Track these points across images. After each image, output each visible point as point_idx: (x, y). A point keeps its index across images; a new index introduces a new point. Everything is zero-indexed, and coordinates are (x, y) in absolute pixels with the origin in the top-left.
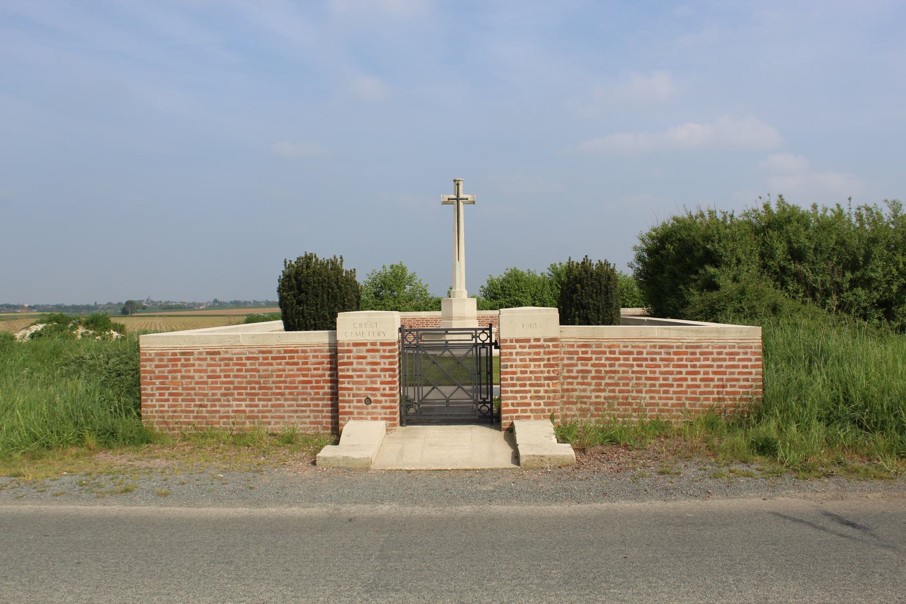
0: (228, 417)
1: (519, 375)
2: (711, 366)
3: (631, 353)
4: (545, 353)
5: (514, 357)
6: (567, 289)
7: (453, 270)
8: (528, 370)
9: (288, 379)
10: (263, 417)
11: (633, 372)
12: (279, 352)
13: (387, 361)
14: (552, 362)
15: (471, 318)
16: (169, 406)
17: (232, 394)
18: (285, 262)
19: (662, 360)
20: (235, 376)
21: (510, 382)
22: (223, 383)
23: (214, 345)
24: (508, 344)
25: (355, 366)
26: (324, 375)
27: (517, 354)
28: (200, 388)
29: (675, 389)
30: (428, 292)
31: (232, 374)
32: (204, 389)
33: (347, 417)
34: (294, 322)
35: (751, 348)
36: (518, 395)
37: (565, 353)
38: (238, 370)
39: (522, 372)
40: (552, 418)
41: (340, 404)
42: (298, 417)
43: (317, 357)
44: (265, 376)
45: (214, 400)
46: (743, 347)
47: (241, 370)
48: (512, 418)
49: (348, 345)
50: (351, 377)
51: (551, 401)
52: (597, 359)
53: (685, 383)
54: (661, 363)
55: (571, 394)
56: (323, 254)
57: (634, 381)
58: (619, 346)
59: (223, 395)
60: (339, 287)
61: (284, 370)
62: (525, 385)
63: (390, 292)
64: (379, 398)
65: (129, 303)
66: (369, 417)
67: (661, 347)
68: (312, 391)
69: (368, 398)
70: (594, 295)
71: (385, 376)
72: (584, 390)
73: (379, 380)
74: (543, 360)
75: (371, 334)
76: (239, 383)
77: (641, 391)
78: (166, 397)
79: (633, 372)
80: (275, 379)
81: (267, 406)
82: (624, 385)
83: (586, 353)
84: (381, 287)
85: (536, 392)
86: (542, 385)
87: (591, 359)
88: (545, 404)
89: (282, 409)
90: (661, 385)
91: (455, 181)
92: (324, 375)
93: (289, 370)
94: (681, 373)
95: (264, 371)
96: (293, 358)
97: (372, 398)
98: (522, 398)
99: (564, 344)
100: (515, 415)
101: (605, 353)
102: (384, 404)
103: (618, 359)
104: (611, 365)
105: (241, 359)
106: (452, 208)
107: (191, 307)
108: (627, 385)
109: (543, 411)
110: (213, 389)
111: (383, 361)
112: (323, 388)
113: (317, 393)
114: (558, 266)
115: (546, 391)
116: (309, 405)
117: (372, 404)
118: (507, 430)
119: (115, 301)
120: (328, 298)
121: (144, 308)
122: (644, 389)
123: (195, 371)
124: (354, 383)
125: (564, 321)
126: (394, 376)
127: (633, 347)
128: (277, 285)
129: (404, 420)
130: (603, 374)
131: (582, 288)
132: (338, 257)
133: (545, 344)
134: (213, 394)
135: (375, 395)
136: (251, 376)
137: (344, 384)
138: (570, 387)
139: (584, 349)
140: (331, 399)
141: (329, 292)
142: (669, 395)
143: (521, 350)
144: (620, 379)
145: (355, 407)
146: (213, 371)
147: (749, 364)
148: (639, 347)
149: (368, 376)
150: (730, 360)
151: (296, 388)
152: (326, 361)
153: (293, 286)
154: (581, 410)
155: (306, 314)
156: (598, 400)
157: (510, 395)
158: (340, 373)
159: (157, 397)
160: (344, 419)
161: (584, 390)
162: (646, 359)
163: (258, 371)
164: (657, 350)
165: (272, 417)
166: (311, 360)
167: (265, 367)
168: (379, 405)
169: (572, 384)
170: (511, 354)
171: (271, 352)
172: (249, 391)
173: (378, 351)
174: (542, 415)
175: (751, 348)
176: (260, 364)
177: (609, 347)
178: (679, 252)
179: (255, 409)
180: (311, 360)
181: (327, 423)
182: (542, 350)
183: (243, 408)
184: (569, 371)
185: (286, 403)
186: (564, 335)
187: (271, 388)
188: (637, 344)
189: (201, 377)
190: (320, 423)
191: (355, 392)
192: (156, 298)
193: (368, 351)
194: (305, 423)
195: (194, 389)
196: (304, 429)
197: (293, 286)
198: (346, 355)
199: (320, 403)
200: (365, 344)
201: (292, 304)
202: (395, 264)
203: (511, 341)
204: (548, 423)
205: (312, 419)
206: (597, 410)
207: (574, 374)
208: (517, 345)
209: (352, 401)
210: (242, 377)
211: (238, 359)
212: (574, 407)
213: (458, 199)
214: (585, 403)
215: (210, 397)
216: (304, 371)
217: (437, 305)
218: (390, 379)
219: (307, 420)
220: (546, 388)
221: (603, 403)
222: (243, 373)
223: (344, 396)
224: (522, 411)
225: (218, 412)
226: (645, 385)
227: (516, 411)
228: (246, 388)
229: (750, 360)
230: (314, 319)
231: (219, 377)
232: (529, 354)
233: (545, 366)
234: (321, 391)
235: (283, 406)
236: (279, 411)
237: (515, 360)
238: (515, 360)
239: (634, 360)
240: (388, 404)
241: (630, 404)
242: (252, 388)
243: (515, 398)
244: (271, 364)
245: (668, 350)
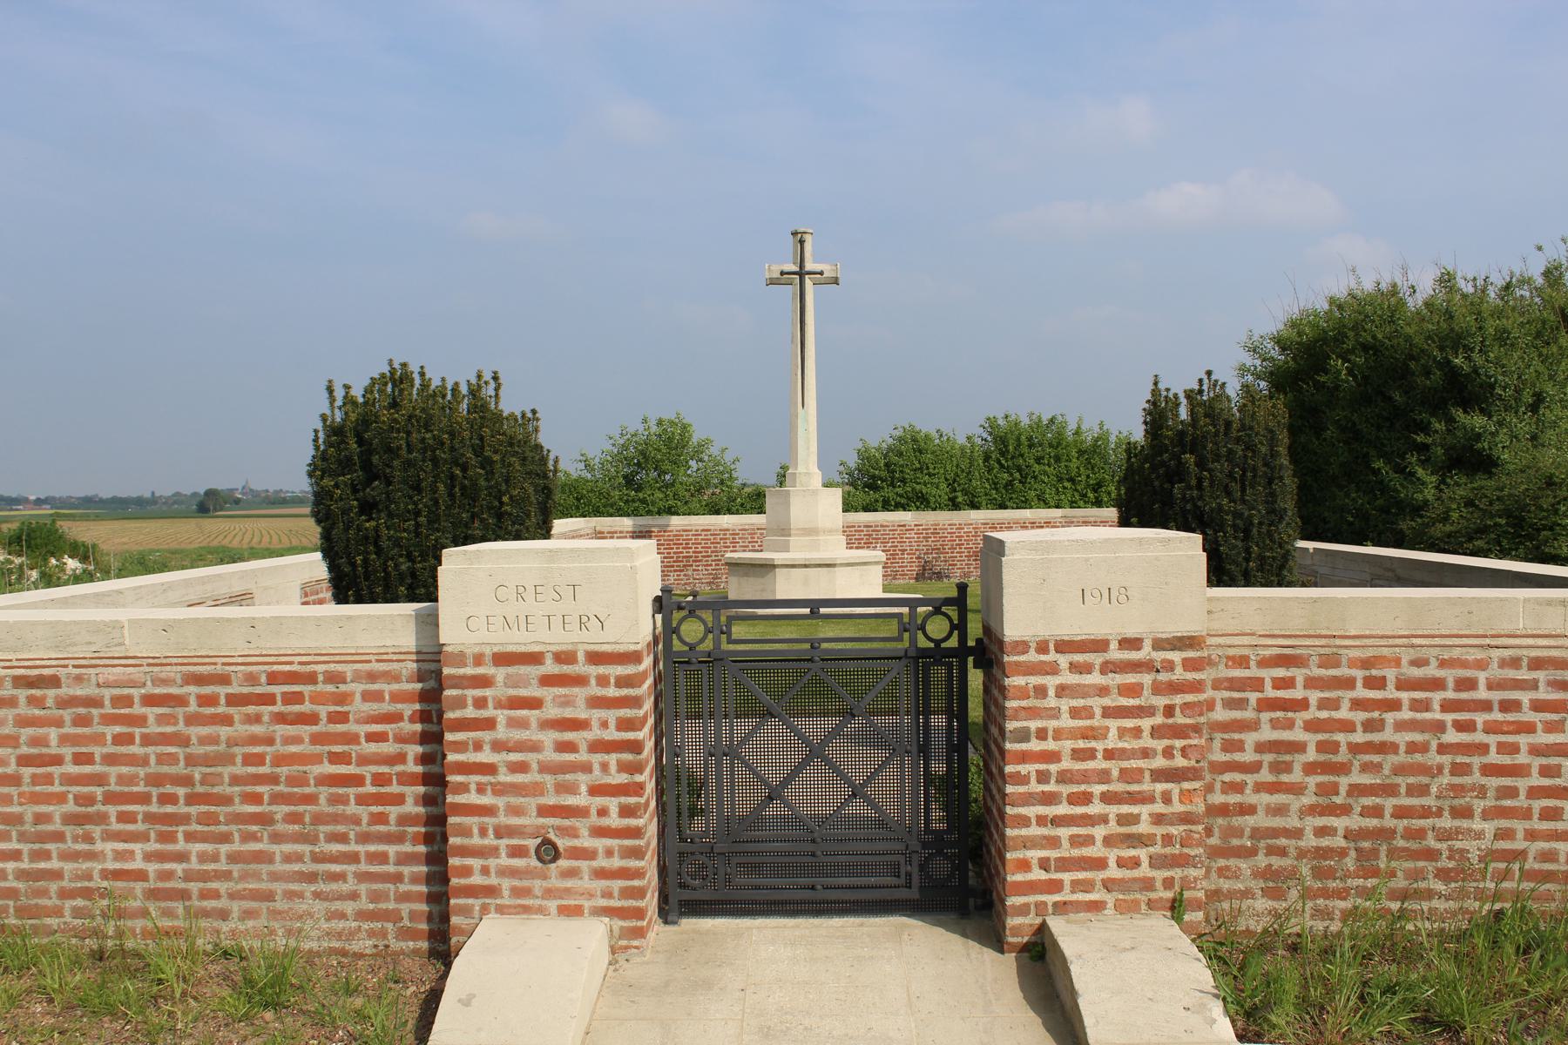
0: (87, 893)
1: (1066, 764)
3: (1437, 684)
4: (1157, 689)
5: (1051, 701)
6: (1154, 468)
7: (793, 428)
8: (1099, 746)
9: (284, 771)
10: (204, 895)
11: (1442, 749)
12: (252, 679)
13: (612, 715)
14: (1180, 719)
15: (831, 531)
17: (102, 818)
18: (330, 390)
19: (1538, 706)
20: (110, 759)
21: (1035, 787)
23: (40, 653)
24: (1032, 656)
25: (501, 732)
26: (400, 758)
27: (1062, 691)
30: (735, 475)
31: (98, 751)
33: (476, 903)
34: (353, 565)
36: (1064, 833)
37: (1217, 685)
38: (119, 740)
39: (1078, 755)
40: (1175, 908)
41: (454, 861)
42: (317, 895)
43: (376, 697)
44: (208, 761)
45: (42, 838)
47: (127, 739)
48: (1041, 908)
49: (478, 660)
50: (490, 769)
51: (1176, 850)
52: (1323, 704)
54: (1536, 717)
55: (1238, 821)
56: (447, 365)
57: (1446, 779)
58: (1397, 662)
59: (70, 819)
60: (487, 463)
61: (270, 741)
62: (1086, 799)
63: (653, 479)
64: (586, 842)
65: (210, 493)
66: (553, 905)
67: (1536, 664)
68: (364, 812)
69: (547, 842)
70: (1235, 487)
71: (605, 767)
72: (1280, 810)
74: (1148, 711)
75: (557, 622)
76: (121, 779)
77: (1466, 813)
79: (1442, 749)
80: (239, 769)
81: (215, 858)
82: (1412, 791)
83: (1288, 683)
84: (639, 464)
85: (1123, 820)
86: (1148, 799)
87: (1303, 704)
88: (1155, 862)
89: (265, 868)
90: (1534, 793)
91: (794, 234)
92: (400, 758)
93: (288, 740)
95: (203, 741)
96: (297, 698)
97: (562, 843)
98: (1076, 841)
99: (1214, 654)
100: (1051, 899)
101: (1349, 683)
102: (601, 862)
103: (1394, 705)
104: (1369, 726)
105: (127, 701)
106: (788, 292)
108: (1423, 790)
109: (1148, 884)
110: (36, 799)
111: (597, 715)
112: (399, 800)
113: (381, 819)
114: (1001, 422)
115: (1158, 819)
116: (353, 858)
117: (563, 863)
118: (1025, 948)
119: (188, 491)
120: (451, 495)
121: (237, 502)
122: (1479, 805)
124: (500, 789)
125: (1219, 574)
126: (636, 768)
127: (1443, 664)
128: (308, 452)
129: (677, 895)
130: (1343, 756)
131: (1201, 464)
132: (487, 376)
133: (1160, 656)
134: (40, 819)
135: (572, 833)
136: (161, 759)
137: (467, 793)
138: (1233, 799)
139: (1281, 672)
140: (428, 839)
141: (452, 477)
144: (1399, 770)
145: (504, 872)
146: (35, 742)
148: (1464, 664)
149: (545, 768)
151: (310, 799)
152: (409, 709)
153: (349, 459)
154: (1267, 874)
155: (384, 544)
156: (1325, 842)
157: (1034, 831)
158: (452, 757)
160: (466, 911)
161: (1280, 810)
162: (1486, 706)
163: (185, 742)
164: (1524, 674)
165: (232, 896)
166: (358, 707)
168: (584, 865)
169: (1238, 788)
170: (1041, 691)
171: (224, 680)
172: (154, 808)
173: (580, 681)
174: (1142, 897)
176: (191, 720)
177: (1366, 664)
178: (1365, 378)
179: (178, 868)
181: (413, 916)
182: (1147, 679)
183: (137, 864)
184: (1229, 747)
185: (277, 849)
186: (1217, 626)
187: (227, 800)
188: (1456, 653)
190: (394, 916)
191: (503, 819)
192: (257, 486)
193: (547, 681)
194: (342, 916)
196: (339, 935)
197: (349, 459)
198: (471, 693)
199: (392, 850)
200: (534, 658)
201: (345, 512)
202: (666, 417)
203: (1042, 648)
204: (1162, 926)
205: (365, 904)
206: (1318, 873)
207: (1248, 756)
208: (1063, 660)
209: (493, 852)
210: (132, 760)
211: (118, 701)
212: (1244, 865)
213: (802, 274)
214: (1282, 852)
215: (29, 827)
216: (337, 744)
217: (755, 502)
218: (623, 778)
219: (349, 907)
220: (1159, 807)
221: (1343, 853)
222: (136, 749)
224: (1077, 885)
225: (57, 875)
226: (1482, 792)
227: (1055, 886)
228: (144, 799)
230: (410, 557)
231: (57, 760)
232: (1103, 691)
233: (1156, 732)
234: (393, 811)
236: (256, 876)
237: (1055, 713)
238: (1055, 713)
239: (1447, 706)
240: (617, 863)
241: (1431, 855)
243: (1054, 842)
244: (227, 720)
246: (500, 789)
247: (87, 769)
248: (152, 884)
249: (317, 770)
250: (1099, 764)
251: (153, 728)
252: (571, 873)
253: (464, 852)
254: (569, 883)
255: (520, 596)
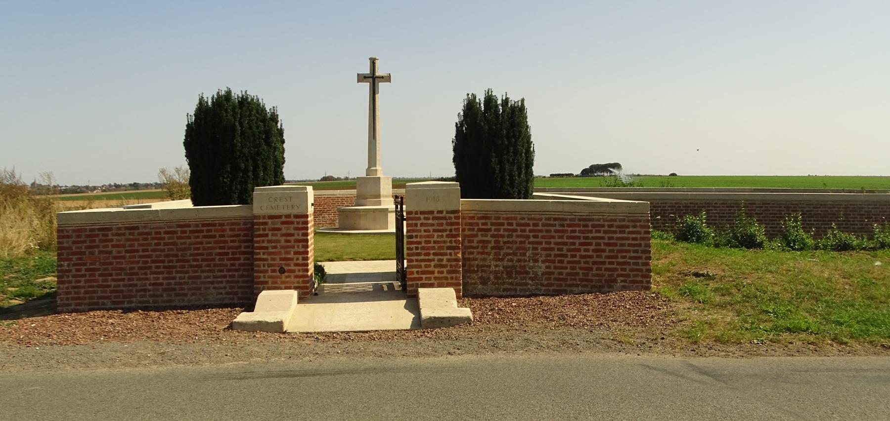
1: (423, 245)
2: (603, 238)
4: (447, 224)
12: (197, 226)
14: (454, 233)
16: (86, 282)
17: (150, 268)
20: (154, 250)
22: (141, 257)
25: (270, 237)
27: (422, 225)
28: (117, 263)
29: (569, 259)
32: (121, 263)
35: (640, 221)
36: (423, 264)
38: (157, 244)
39: (426, 242)
42: (214, 288)
46: (632, 221)
49: (264, 217)
50: (267, 248)
52: (496, 230)
53: (578, 254)
55: (472, 263)
59: (141, 268)
62: (428, 254)
64: (293, 268)
66: (283, 286)
67: (555, 219)
68: (228, 263)
71: (298, 247)
73: (292, 251)
74: (445, 230)
78: (83, 272)
79: (529, 243)
80: (192, 252)
81: (184, 278)
83: (485, 224)
86: (446, 254)
87: (490, 230)
89: (198, 280)
90: (556, 256)
93: (207, 243)
94: (574, 244)
95: (182, 244)
97: (286, 268)
98: (426, 266)
100: (420, 282)
101: (503, 224)
102: (297, 273)
103: (516, 230)
104: (508, 236)
105: (159, 233)
107: (383, 77)
113: (234, 265)
115: (449, 260)
116: (225, 276)
117: (286, 274)
123: (113, 246)
124: (270, 254)
127: (529, 219)
134: (131, 268)
135: (289, 265)
136: (169, 250)
139: (484, 221)
142: (564, 265)
143: (425, 222)
145: (269, 277)
147: (639, 236)
148: (534, 219)
149: (282, 247)
150: (621, 232)
151: (213, 260)
154: (481, 278)
159: (74, 272)
164: (552, 222)
165: (189, 289)
167: (182, 241)
168: (292, 274)
170: (416, 225)
171: (189, 226)
172: (166, 264)
173: (292, 223)
175: (640, 221)
176: (178, 238)
177: (507, 219)
180: (229, 232)
182: (444, 222)
187: (188, 261)
189: (119, 252)
191: (270, 262)
193: (283, 223)
194: (221, 294)
195: (111, 263)
196: (220, 300)
199: (236, 274)
200: (279, 217)
203: (416, 213)
207: (475, 244)
208: (422, 216)
209: (266, 271)
210: (160, 250)
211: (156, 233)
214: (485, 271)
219: (223, 291)
220: (449, 257)
222: (161, 247)
223: (259, 266)
225: (136, 285)
227: (421, 279)
228: (163, 262)
229: (639, 233)
231: (137, 251)
232: (433, 225)
233: (448, 236)
234: (237, 262)
235: (200, 277)
239: (531, 231)
240: (301, 273)
242: (170, 261)
243: (420, 266)
244: (189, 238)
245: (562, 222)
246: (270, 254)
247: (146, 253)
248: (165, 287)
249: (215, 251)
250: (432, 245)
251: (167, 241)
252: (288, 277)
253: (259, 272)
254: (288, 279)
255: (276, 200)
